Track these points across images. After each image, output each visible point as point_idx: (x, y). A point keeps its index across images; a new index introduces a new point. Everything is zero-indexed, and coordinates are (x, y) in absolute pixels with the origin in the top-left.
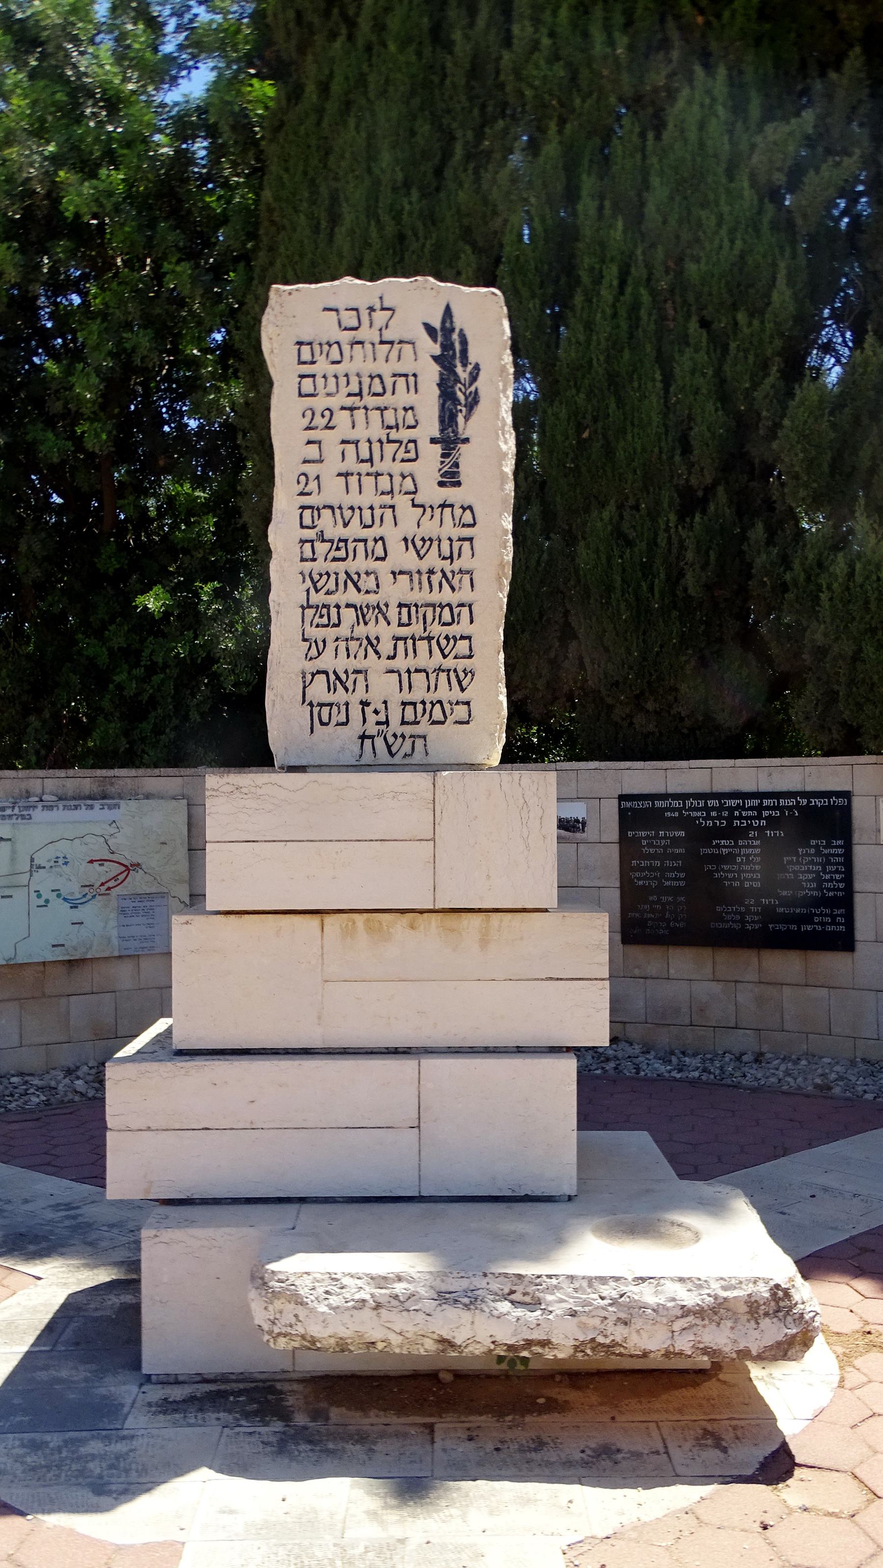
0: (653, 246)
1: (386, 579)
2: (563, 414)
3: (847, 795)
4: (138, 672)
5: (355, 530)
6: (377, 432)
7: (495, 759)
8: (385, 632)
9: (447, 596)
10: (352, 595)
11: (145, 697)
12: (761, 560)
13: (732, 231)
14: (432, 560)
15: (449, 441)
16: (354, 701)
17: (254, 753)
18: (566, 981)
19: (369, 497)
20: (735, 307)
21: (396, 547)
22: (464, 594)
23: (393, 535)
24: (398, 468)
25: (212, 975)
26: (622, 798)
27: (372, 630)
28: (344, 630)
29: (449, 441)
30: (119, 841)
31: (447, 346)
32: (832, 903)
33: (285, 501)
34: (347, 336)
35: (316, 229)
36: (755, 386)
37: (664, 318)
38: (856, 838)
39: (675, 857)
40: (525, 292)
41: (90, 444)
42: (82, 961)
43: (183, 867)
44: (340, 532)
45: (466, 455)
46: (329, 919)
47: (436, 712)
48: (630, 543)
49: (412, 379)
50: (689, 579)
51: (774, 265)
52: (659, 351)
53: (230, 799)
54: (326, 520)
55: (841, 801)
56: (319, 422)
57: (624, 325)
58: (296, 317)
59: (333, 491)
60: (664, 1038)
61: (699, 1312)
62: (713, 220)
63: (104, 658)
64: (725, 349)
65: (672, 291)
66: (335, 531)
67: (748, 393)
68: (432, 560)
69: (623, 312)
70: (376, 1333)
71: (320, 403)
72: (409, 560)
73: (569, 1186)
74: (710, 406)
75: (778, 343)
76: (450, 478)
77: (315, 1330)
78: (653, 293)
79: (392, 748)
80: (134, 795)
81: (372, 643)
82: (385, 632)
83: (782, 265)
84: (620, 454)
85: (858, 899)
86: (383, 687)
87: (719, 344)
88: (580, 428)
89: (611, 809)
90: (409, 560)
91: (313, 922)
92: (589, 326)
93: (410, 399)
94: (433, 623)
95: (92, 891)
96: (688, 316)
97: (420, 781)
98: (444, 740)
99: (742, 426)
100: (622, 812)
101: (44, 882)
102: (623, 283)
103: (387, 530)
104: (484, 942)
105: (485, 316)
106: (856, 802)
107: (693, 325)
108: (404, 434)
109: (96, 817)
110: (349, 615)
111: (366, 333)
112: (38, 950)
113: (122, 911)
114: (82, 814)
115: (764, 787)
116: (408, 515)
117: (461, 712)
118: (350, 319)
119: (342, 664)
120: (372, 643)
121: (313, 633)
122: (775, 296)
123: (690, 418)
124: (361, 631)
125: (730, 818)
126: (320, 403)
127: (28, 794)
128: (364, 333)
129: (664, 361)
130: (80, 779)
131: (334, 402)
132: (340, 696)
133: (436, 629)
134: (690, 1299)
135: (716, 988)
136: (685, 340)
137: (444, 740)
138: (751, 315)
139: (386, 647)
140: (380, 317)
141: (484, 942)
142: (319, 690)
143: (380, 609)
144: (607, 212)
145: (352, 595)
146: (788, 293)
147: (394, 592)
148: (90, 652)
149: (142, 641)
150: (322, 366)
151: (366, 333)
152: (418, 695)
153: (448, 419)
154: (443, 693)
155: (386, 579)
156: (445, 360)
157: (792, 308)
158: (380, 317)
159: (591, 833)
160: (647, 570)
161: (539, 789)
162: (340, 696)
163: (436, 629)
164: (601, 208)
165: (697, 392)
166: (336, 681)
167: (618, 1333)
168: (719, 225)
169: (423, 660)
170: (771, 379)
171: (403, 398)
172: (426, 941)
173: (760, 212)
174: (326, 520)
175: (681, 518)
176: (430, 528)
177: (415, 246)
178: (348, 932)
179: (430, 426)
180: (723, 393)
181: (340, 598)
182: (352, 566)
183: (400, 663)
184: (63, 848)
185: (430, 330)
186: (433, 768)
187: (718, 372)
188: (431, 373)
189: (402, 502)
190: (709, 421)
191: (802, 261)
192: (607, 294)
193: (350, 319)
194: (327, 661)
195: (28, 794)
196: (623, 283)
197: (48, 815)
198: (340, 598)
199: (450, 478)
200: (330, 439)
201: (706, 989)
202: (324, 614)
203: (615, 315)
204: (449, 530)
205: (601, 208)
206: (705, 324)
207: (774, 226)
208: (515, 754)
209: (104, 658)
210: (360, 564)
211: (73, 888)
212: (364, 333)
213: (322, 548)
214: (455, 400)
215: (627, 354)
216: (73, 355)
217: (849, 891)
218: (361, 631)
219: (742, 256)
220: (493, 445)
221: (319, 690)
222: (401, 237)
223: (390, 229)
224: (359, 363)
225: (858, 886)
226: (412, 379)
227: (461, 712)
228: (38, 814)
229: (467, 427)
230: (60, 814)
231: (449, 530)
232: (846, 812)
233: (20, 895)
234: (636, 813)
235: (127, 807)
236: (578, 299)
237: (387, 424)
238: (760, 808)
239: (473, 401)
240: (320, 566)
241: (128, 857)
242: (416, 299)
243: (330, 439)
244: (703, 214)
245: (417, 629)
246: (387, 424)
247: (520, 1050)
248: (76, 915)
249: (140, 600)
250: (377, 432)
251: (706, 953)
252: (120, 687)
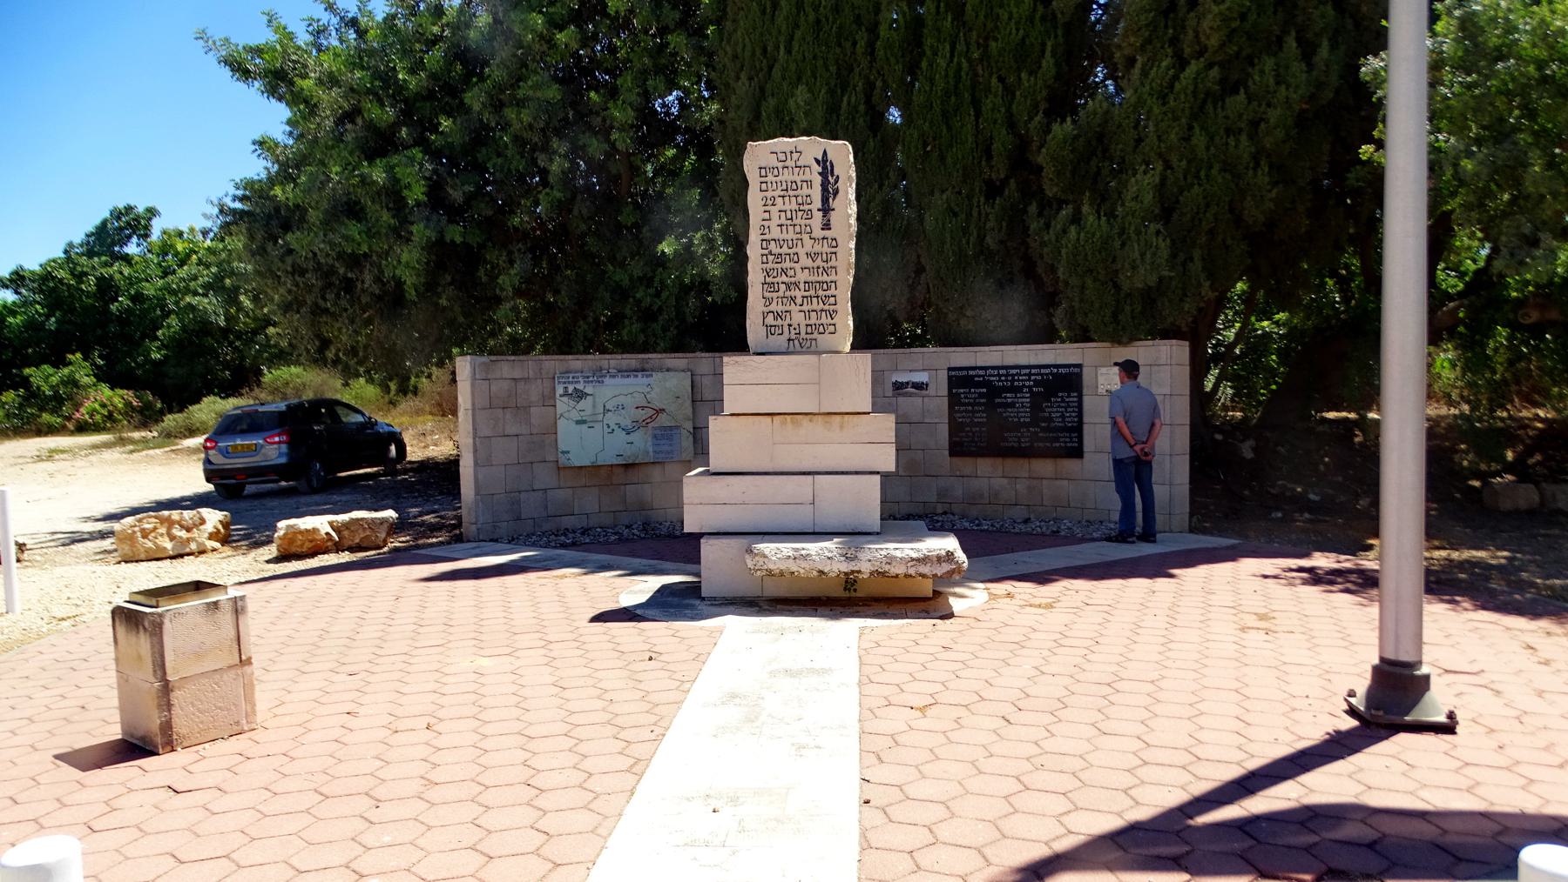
0: (970, 30)
1: (799, 271)
2: (916, 135)
3: (1080, 366)
4: (652, 291)
5: (785, 250)
6: (794, 206)
7: (848, 348)
8: (798, 294)
9: (825, 278)
10: (784, 278)
11: (655, 308)
12: (1034, 226)
13: (1018, 23)
14: (819, 262)
15: (826, 209)
16: (786, 324)
17: (739, 344)
18: (874, 445)
19: (791, 235)
20: (1019, 70)
21: (803, 257)
22: (833, 277)
23: (802, 252)
24: (803, 222)
25: (727, 439)
26: (950, 369)
27: (792, 293)
28: (781, 294)
29: (826, 209)
30: (652, 395)
31: (825, 168)
32: (1070, 430)
33: (754, 237)
34: (780, 165)
35: (764, 12)
36: (1031, 119)
37: (976, 75)
38: (1085, 391)
39: (980, 404)
40: (892, 60)
41: (620, 146)
42: (633, 465)
43: (689, 411)
44: (779, 250)
45: (833, 216)
46: (776, 418)
47: (821, 329)
48: (955, 215)
49: (809, 183)
50: (988, 240)
51: (1044, 45)
52: (973, 96)
53: (734, 367)
54: (773, 245)
55: (1076, 370)
56: (769, 203)
57: (952, 82)
58: (759, 155)
59: (775, 233)
60: (974, 511)
61: (918, 560)
62: (1006, 16)
63: (626, 282)
64: (1014, 95)
65: (981, 60)
66: (777, 251)
67: (1026, 123)
68: (819, 262)
69: (951, 74)
70: (794, 569)
71: (769, 194)
72: (809, 263)
73: (877, 528)
74: (1004, 132)
75: (1044, 93)
76: (827, 226)
77: (771, 567)
78: (969, 61)
79: (801, 344)
80: (660, 370)
81: (793, 299)
82: (798, 294)
83: (1049, 44)
84: (949, 160)
85: (1086, 428)
86: (798, 318)
87: (1009, 91)
88: (925, 144)
89: (943, 376)
90: (809, 263)
91: (768, 419)
92: (932, 81)
93: (809, 191)
94: (820, 290)
95: (638, 425)
96: (991, 75)
97: (812, 358)
98: (824, 340)
99: (1023, 144)
100: (950, 378)
101: (611, 419)
102: (952, 55)
103: (799, 250)
104: (841, 427)
105: (842, 153)
106: (1085, 370)
107: (994, 80)
108: (806, 207)
109: (638, 383)
110: (783, 287)
111: (789, 163)
112: (609, 458)
113: (655, 436)
114: (631, 380)
115: (1033, 362)
116: (808, 242)
117: (832, 328)
118: (782, 157)
119: (780, 308)
120: (793, 299)
121: (767, 295)
122: (1044, 63)
123: (991, 138)
124: (788, 294)
125: (1013, 381)
126: (769, 194)
127: (601, 369)
128: (789, 163)
129: (976, 103)
130: (631, 360)
131: (776, 194)
132: (779, 322)
133: (821, 293)
134: (915, 555)
135: (1005, 481)
136: (988, 90)
137: (824, 340)
138: (1030, 74)
139: (799, 301)
140: (795, 156)
141: (841, 427)
142: (770, 320)
143: (796, 284)
144: (942, 10)
145: (784, 278)
146: (1052, 61)
147: (802, 277)
148: (617, 278)
149: (654, 271)
150: (770, 178)
151: (789, 163)
152: (812, 321)
153: (825, 200)
154: (824, 320)
155: (799, 271)
156: (823, 174)
157: (1053, 71)
158: (795, 156)
159: (931, 391)
160: (965, 231)
161: (865, 359)
162: (779, 322)
163: (821, 293)
164: (938, 7)
165: (995, 122)
166: (778, 316)
167: (887, 568)
168: (1010, 19)
169: (815, 306)
170: (1038, 119)
171: (805, 191)
172: (815, 428)
173: (1035, 10)
174: (773, 245)
175: (987, 198)
176: (818, 248)
177: (826, 28)
178: (784, 423)
179: (818, 203)
180: (1011, 124)
181: (779, 279)
182: (784, 265)
183: (805, 307)
184: (621, 400)
185: (817, 161)
186: (819, 353)
187: (1009, 110)
188: (818, 180)
189: (806, 237)
190: (1002, 142)
191: (1061, 40)
192: (942, 63)
193: (782, 157)
194: (773, 307)
195: (601, 369)
196: (952, 55)
197: (613, 381)
198: (779, 279)
199: (827, 226)
200: (774, 210)
201: (999, 482)
202: (769, 286)
203: (947, 76)
204: (826, 249)
205: (938, 7)
206: (1001, 80)
207: (1043, 19)
208: (860, 344)
209: (626, 282)
210: (788, 264)
211: (627, 423)
212: (789, 163)
213: (771, 258)
214: (829, 192)
215: (953, 99)
216: (613, 92)
217: (1081, 422)
218: (788, 294)
219: (1023, 39)
220: (847, 207)
221: (770, 320)
222: (818, 21)
223: (812, 17)
224: (786, 176)
225: (1086, 419)
226: (809, 183)
227: (832, 328)
228: (607, 380)
229: (834, 204)
230: (618, 380)
231: (826, 249)
232: (1079, 376)
233: (598, 426)
234: (960, 380)
235: (657, 376)
236: (924, 64)
237: (799, 199)
238: (1030, 375)
239: (836, 192)
240: (770, 265)
241: (658, 405)
242: (810, 147)
243: (774, 210)
244: (1000, 11)
245: (812, 292)
246: (799, 199)
247: (857, 473)
248: (630, 438)
249: (660, 247)
250: (794, 206)
251: (999, 461)
252: (639, 301)
